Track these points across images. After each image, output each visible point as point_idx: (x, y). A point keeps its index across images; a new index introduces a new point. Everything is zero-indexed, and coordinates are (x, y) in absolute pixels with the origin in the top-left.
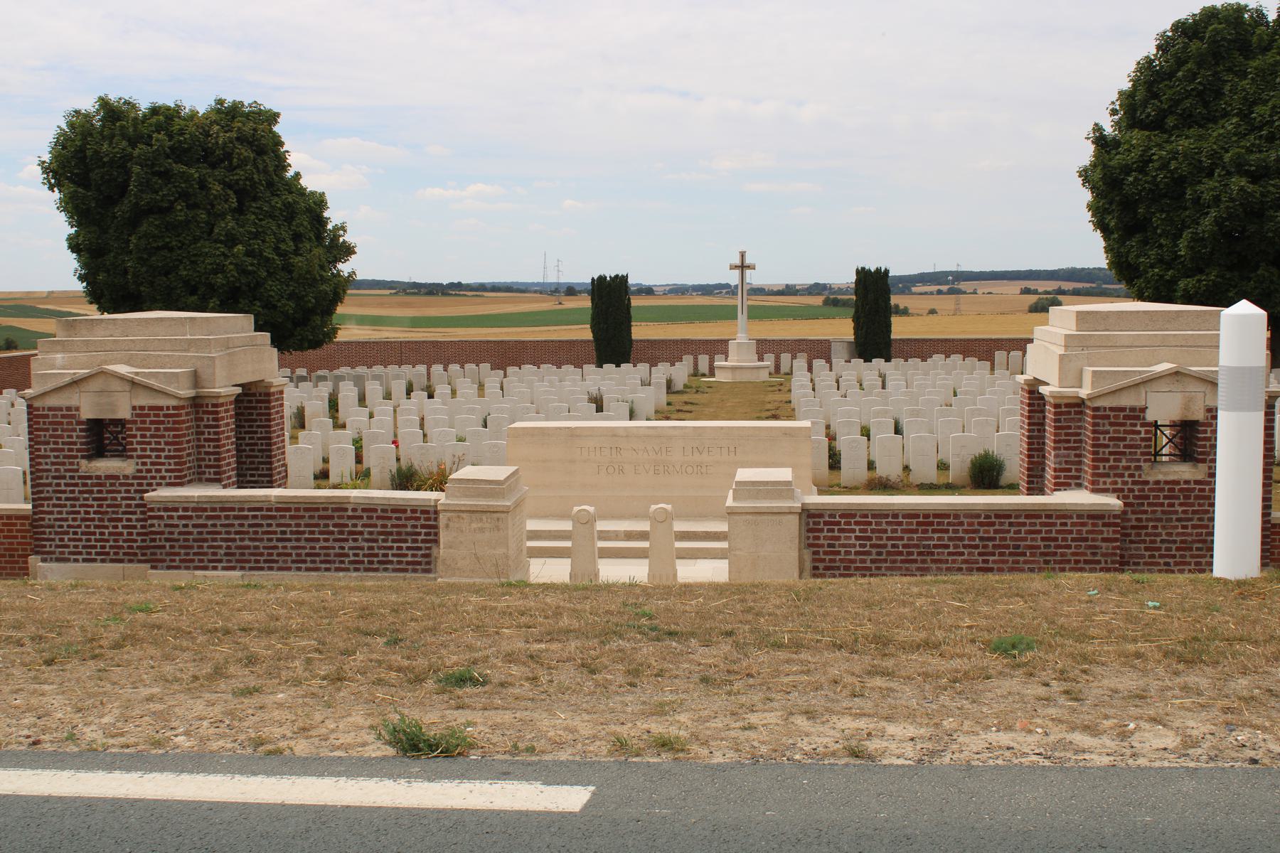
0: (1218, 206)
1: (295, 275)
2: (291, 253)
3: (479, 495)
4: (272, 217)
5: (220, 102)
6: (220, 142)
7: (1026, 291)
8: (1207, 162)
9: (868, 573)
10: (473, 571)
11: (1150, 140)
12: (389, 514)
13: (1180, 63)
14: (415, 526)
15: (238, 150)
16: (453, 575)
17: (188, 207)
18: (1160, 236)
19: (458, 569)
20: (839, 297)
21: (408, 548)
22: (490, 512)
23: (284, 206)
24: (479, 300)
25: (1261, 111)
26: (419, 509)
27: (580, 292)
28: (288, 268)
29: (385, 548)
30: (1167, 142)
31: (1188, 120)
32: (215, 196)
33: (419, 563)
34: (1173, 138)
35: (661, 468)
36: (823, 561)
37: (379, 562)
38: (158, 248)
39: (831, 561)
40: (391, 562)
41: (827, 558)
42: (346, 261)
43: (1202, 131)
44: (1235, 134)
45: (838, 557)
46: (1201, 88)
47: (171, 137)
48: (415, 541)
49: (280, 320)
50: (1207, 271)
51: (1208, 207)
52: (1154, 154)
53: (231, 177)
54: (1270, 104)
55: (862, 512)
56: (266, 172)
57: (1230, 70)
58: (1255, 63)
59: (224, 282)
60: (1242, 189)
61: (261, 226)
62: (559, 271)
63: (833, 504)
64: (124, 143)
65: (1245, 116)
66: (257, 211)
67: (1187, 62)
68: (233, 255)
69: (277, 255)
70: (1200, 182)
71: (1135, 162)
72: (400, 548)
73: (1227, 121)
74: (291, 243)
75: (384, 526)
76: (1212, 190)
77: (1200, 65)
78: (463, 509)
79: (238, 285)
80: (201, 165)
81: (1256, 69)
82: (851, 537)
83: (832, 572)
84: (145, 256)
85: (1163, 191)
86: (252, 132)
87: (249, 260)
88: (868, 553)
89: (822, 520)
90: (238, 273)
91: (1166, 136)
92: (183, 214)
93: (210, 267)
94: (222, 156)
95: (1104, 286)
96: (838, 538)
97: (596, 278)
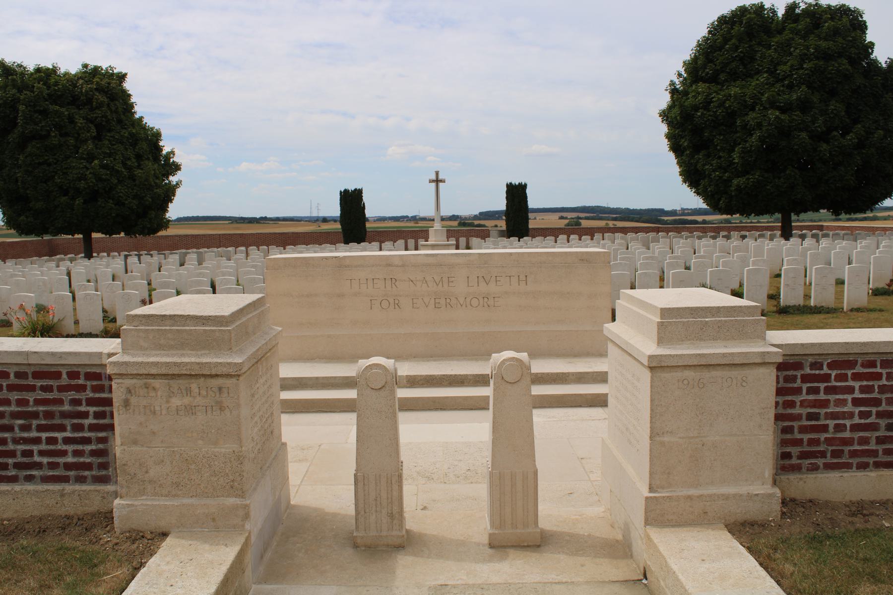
0: (761, 129)
1: (137, 182)
2: (135, 168)
3: (182, 345)
4: (122, 143)
5: (85, 66)
6: (84, 91)
7: (562, 218)
8: (750, 101)
9: (871, 461)
10: (178, 485)
11: (710, 88)
12: (31, 381)
13: (726, 40)
14: (76, 402)
15: (96, 97)
16: (142, 492)
17: (61, 135)
18: (719, 151)
19: (150, 481)
20: (466, 221)
21: (67, 441)
22: (204, 376)
23: (130, 135)
24: (274, 225)
25: (783, 69)
26: (83, 371)
27: (330, 221)
28: (133, 178)
29: (26, 441)
30: (721, 90)
31: (734, 76)
32: (80, 127)
33: (88, 467)
34: (725, 88)
35: (443, 301)
36: (798, 442)
37: (17, 466)
38: (40, 164)
39: (811, 442)
40: (39, 466)
41: (806, 437)
42: (174, 175)
43: (744, 83)
44: (767, 84)
45: (823, 436)
46: (742, 55)
47: (49, 87)
48: (78, 428)
49: (127, 213)
50: (752, 172)
51: (754, 129)
52: (713, 98)
53: (92, 115)
54: (789, 64)
55: (868, 358)
56: (116, 112)
57: (759, 44)
58: (776, 40)
59: (86, 186)
60: (777, 117)
61: (114, 149)
62: (318, 209)
63: (821, 344)
64: (14, 91)
65: (772, 73)
66: (111, 139)
67: (732, 39)
68: (92, 167)
69: (125, 169)
70: (747, 114)
71: (701, 103)
72: (52, 441)
73: (761, 76)
74: (134, 160)
75: (22, 402)
76: (756, 118)
77: (740, 40)
78: (154, 371)
79: (96, 188)
80: (70, 107)
81: (776, 43)
82: (845, 400)
83: (813, 461)
84: (30, 169)
85: (721, 121)
86: (107, 85)
87: (103, 171)
88: (873, 427)
89: (799, 374)
90: (96, 180)
91: (719, 87)
92: (56, 139)
93: (76, 176)
94: (85, 101)
95: (600, 215)
96: (825, 404)
97: (342, 191)
